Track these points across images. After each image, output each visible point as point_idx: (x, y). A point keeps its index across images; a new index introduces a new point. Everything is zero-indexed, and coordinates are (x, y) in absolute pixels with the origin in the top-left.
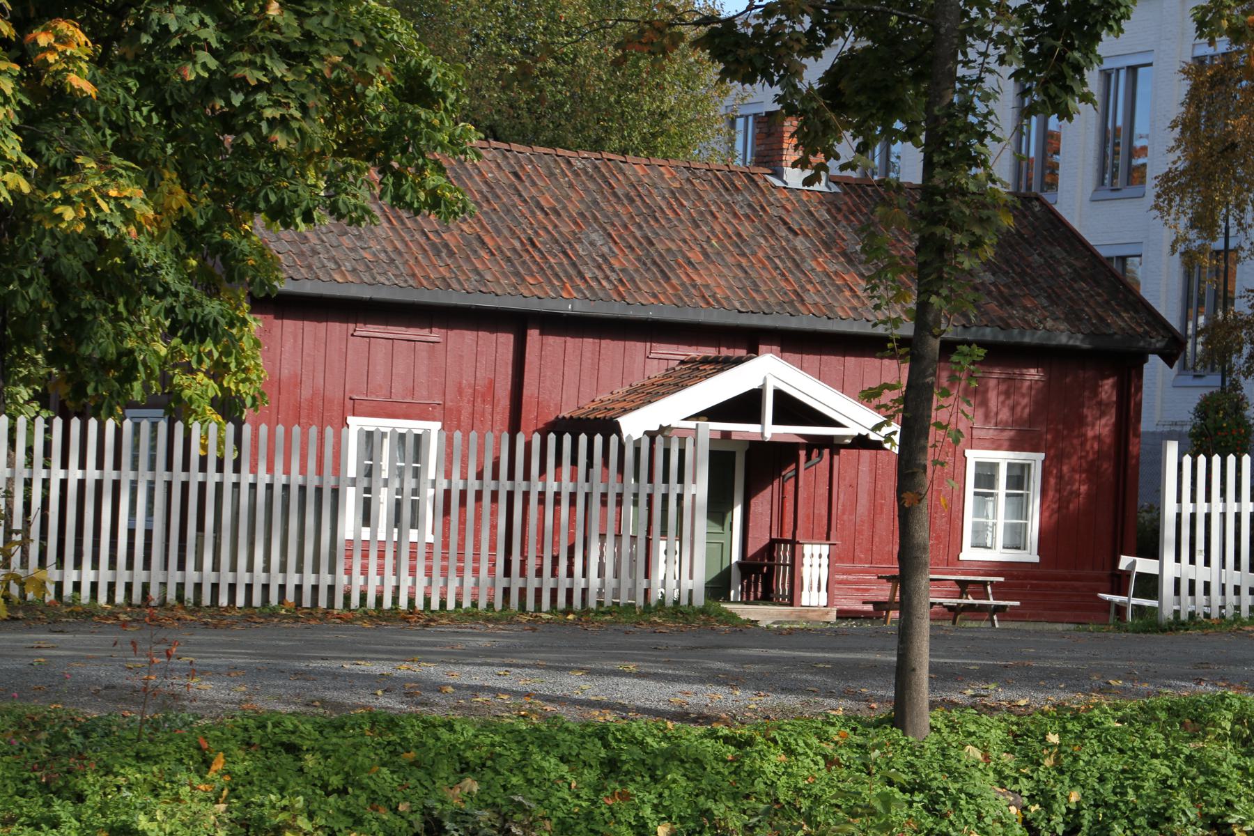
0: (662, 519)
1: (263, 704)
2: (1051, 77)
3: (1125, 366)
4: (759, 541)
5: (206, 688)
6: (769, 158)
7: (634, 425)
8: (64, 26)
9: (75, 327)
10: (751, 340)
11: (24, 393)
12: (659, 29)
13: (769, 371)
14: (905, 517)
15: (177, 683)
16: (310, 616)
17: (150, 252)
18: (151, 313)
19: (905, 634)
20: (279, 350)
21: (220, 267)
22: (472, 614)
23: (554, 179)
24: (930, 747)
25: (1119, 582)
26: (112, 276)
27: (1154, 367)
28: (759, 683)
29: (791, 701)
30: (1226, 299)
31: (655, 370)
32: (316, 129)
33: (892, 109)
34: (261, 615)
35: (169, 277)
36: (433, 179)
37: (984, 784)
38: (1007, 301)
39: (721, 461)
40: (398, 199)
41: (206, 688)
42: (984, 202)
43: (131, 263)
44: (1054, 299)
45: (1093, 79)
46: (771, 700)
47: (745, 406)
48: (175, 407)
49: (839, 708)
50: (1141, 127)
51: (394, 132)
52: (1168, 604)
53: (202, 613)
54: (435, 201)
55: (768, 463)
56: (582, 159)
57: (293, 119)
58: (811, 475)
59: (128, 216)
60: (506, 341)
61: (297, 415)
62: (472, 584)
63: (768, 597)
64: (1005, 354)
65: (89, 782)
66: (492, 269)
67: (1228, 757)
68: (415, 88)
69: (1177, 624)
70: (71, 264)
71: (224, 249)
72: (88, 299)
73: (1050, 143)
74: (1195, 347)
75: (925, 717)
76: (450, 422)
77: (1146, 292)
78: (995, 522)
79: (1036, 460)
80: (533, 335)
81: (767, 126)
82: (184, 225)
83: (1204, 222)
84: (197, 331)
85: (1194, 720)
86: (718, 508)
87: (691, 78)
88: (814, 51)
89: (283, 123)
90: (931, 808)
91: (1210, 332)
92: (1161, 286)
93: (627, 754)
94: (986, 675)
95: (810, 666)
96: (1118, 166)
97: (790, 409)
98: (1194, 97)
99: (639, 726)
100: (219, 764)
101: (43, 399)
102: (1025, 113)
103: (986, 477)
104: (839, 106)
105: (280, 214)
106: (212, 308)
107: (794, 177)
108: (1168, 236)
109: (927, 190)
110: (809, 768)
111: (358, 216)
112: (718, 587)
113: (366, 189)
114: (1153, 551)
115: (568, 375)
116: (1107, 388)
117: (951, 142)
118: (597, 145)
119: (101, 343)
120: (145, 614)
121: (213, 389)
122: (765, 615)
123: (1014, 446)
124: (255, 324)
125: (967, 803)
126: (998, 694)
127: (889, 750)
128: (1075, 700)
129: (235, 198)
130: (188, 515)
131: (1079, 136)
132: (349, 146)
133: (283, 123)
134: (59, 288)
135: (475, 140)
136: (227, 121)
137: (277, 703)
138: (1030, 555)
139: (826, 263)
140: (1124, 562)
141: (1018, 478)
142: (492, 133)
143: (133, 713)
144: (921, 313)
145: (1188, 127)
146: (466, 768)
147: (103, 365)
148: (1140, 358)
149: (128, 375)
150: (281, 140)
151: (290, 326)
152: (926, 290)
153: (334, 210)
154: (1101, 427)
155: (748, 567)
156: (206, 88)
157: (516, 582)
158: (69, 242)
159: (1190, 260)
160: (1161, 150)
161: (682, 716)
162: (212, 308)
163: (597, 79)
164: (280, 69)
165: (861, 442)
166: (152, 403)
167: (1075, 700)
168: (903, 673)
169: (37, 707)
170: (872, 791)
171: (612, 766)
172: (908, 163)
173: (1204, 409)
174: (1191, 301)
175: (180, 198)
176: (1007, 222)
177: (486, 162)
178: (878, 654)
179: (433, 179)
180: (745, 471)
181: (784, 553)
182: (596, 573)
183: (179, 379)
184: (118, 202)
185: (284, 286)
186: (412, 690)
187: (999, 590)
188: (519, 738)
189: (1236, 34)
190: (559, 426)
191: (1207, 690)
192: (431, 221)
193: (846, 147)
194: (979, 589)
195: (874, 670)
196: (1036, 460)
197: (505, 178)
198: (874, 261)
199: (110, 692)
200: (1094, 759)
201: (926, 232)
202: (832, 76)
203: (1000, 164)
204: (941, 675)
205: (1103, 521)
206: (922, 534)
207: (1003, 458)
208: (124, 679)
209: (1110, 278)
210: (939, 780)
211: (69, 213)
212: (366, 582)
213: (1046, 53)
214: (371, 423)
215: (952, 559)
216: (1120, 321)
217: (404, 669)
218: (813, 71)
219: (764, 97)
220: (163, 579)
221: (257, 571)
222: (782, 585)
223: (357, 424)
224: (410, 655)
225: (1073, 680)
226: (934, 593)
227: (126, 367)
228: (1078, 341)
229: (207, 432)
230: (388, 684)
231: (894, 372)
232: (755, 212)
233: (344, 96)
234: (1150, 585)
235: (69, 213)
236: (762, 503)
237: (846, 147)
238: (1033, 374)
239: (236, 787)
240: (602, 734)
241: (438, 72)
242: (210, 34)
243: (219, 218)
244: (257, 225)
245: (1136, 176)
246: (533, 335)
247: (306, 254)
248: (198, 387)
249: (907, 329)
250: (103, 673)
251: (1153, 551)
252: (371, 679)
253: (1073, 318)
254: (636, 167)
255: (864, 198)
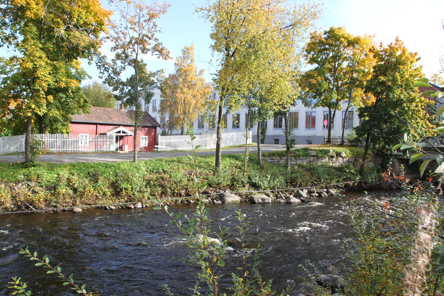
0: (111, 143)
1: (72, 162)
2: (148, 101)
3: (155, 128)
4: (121, 145)
5: (66, 160)
6: (121, 108)
7: (108, 134)
8: (50, 96)
9: (52, 125)
10: (120, 125)
11: (47, 132)
12: (109, 96)
13: (121, 129)
14: (134, 142)
15: (63, 160)
16: (76, 153)
17: (59, 118)
18: (60, 124)
19: (135, 153)
20: (72, 127)
21: (66, 119)
22: (92, 153)
23: (100, 110)
24: (137, 164)
25: (155, 148)
26: (56, 120)
27: (158, 128)
28: (120, 158)
29: (124, 160)
30: (164, 121)
31: (110, 129)
32: (75, 105)
33: (132, 103)
34: (71, 153)
35: (61, 120)
36: (87, 110)
37: (142, 167)
38: (144, 122)
39: (117, 137)
40: (84, 112)
41: (66, 160)
42: (142, 113)
43: (57, 119)
44: (149, 121)
45: (151, 101)
46: (122, 160)
47: (119, 132)
48: (62, 133)
49: (128, 161)
50: (156, 106)
51: (83, 106)
52: (159, 150)
53: (66, 153)
54: (88, 112)
55: (122, 137)
56: (103, 108)
57: (72, 104)
58: (126, 138)
59: (57, 114)
60: (95, 126)
61: (74, 133)
62: (93, 149)
63: (122, 150)
64: (143, 127)
65: (55, 169)
66: (94, 119)
67: (164, 163)
68: (85, 101)
69: (160, 152)
70: (51, 119)
71: (67, 117)
72: (53, 122)
73: (148, 107)
74: (162, 126)
75: (137, 161)
76: (90, 133)
77: (157, 121)
78: (143, 142)
79: (147, 137)
80: (98, 125)
81: (121, 105)
82: (63, 115)
83: (162, 115)
84: (64, 125)
85: (161, 160)
86: (117, 141)
87: (113, 100)
88: (125, 97)
89: (72, 105)
90: (137, 170)
91: (163, 125)
92: (158, 121)
93: (108, 165)
94: (142, 157)
95: (125, 157)
96: (154, 109)
97: (124, 132)
98: (161, 103)
99: (109, 163)
100: (67, 167)
101: (49, 132)
102: (145, 104)
103: (143, 139)
104: (127, 103)
105: (72, 114)
106: (65, 123)
107: (123, 110)
108: (159, 116)
109: (136, 111)
110: (126, 166)
111: (80, 114)
112: (117, 150)
113: (81, 111)
114: (157, 145)
115: (101, 129)
116: (154, 130)
117: (138, 106)
118: (104, 107)
119: (54, 127)
120: (60, 153)
121: (66, 131)
122: (121, 152)
123: (145, 135)
124: (70, 125)
125: (164, 273)
126: (143, 159)
127: (134, 164)
128: (151, 159)
129: (67, 112)
130: (64, 143)
131: (150, 106)
132: (79, 107)
133: (72, 105)
134: (50, 121)
135: (92, 106)
136: (67, 105)
137: (73, 162)
138: (147, 146)
139: (127, 118)
140: (155, 146)
141: (146, 139)
142: (94, 106)
143: (59, 163)
144: (136, 123)
145: (160, 106)
146: (92, 167)
147: (55, 129)
148: (156, 127)
149: (58, 130)
150: (72, 107)
151: (74, 125)
152: (136, 120)
153: (78, 113)
154: (153, 133)
155: (120, 148)
156: (64, 102)
157: (97, 149)
158: (51, 117)
159: (161, 118)
160: (158, 108)
161: (113, 162)
162: (65, 123)
163: (104, 101)
164: (71, 100)
165: (131, 135)
166: (60, 133)
167: (151, 159)
168: (134, 157)
169: (49, 162)
170: (131, 168)
171: (106, 167)
172: (134, 108)
173: (162, 132)
174: (161, 122)
175: (62, 112)
176: (143, 114)
177: (93, 108)
178: (132, 156)
179: (87, 110)
180: (119, 138)
181: (123, 146)
182: (105, 149)
183: (62, 130)
184: (55, 113)
185: (73, 121)
186: (86, 160)
187: (144, 149)
188: (97, 164)
189: (164, 97)
190: (101, 134)
191: (162, 157)
192: (87, 114)
193: (128, 107)
194: (142, 149)
195: (132, 157)
196: (147, 137)
197: (95, 110)
198: (131, 117)
199: (56, 161)
200: (152, 164)
201: (136, 115)
202: (127, 100)
203: (143, 109)
204: (138, 157)
205: (153, 142)
206: (136, 144)
207: (144, 137)
208: (57, 159)
209: (154, 120)
210: (138, 167)
211: (51, 114)
212: (81, 150)
213: (147, 99)
214: (82, 134)
215: (139, 146)
216: (155, 124)
217: (85, 158)
218: (125, 100)
219: (120, 102)
220: (61, 150)
221: (70, 149)
222: (123, 149)
223: (81, 134)
224: (86, 157)
225: (150, 157)
226: (137, 149)
227: (57, 129)
228: (151, 125)
229: (65, 135)
230: (84, 160)
231: (133, 128)
232: (120, 113)
233: (78, 102)
234: (157, 148)
235: (51, 114)
236: (121, 141)
237: (128, 107)
238: (147, 129)
239: (69, 170)
240: (105, 164)
241: (88, 100)
242: (65, 97)
243: (66, 114)
244: (70, 115)
245: (156, 110)
246: (98, 125)
247: (75, 117)
248: (64, 131)
249: (134, 124)
250: (56, 159)
251: (157, 145)
252: (82, 159)
253: (150, 123)
254: (108, 109)
255: (130, 112)
